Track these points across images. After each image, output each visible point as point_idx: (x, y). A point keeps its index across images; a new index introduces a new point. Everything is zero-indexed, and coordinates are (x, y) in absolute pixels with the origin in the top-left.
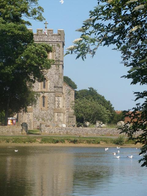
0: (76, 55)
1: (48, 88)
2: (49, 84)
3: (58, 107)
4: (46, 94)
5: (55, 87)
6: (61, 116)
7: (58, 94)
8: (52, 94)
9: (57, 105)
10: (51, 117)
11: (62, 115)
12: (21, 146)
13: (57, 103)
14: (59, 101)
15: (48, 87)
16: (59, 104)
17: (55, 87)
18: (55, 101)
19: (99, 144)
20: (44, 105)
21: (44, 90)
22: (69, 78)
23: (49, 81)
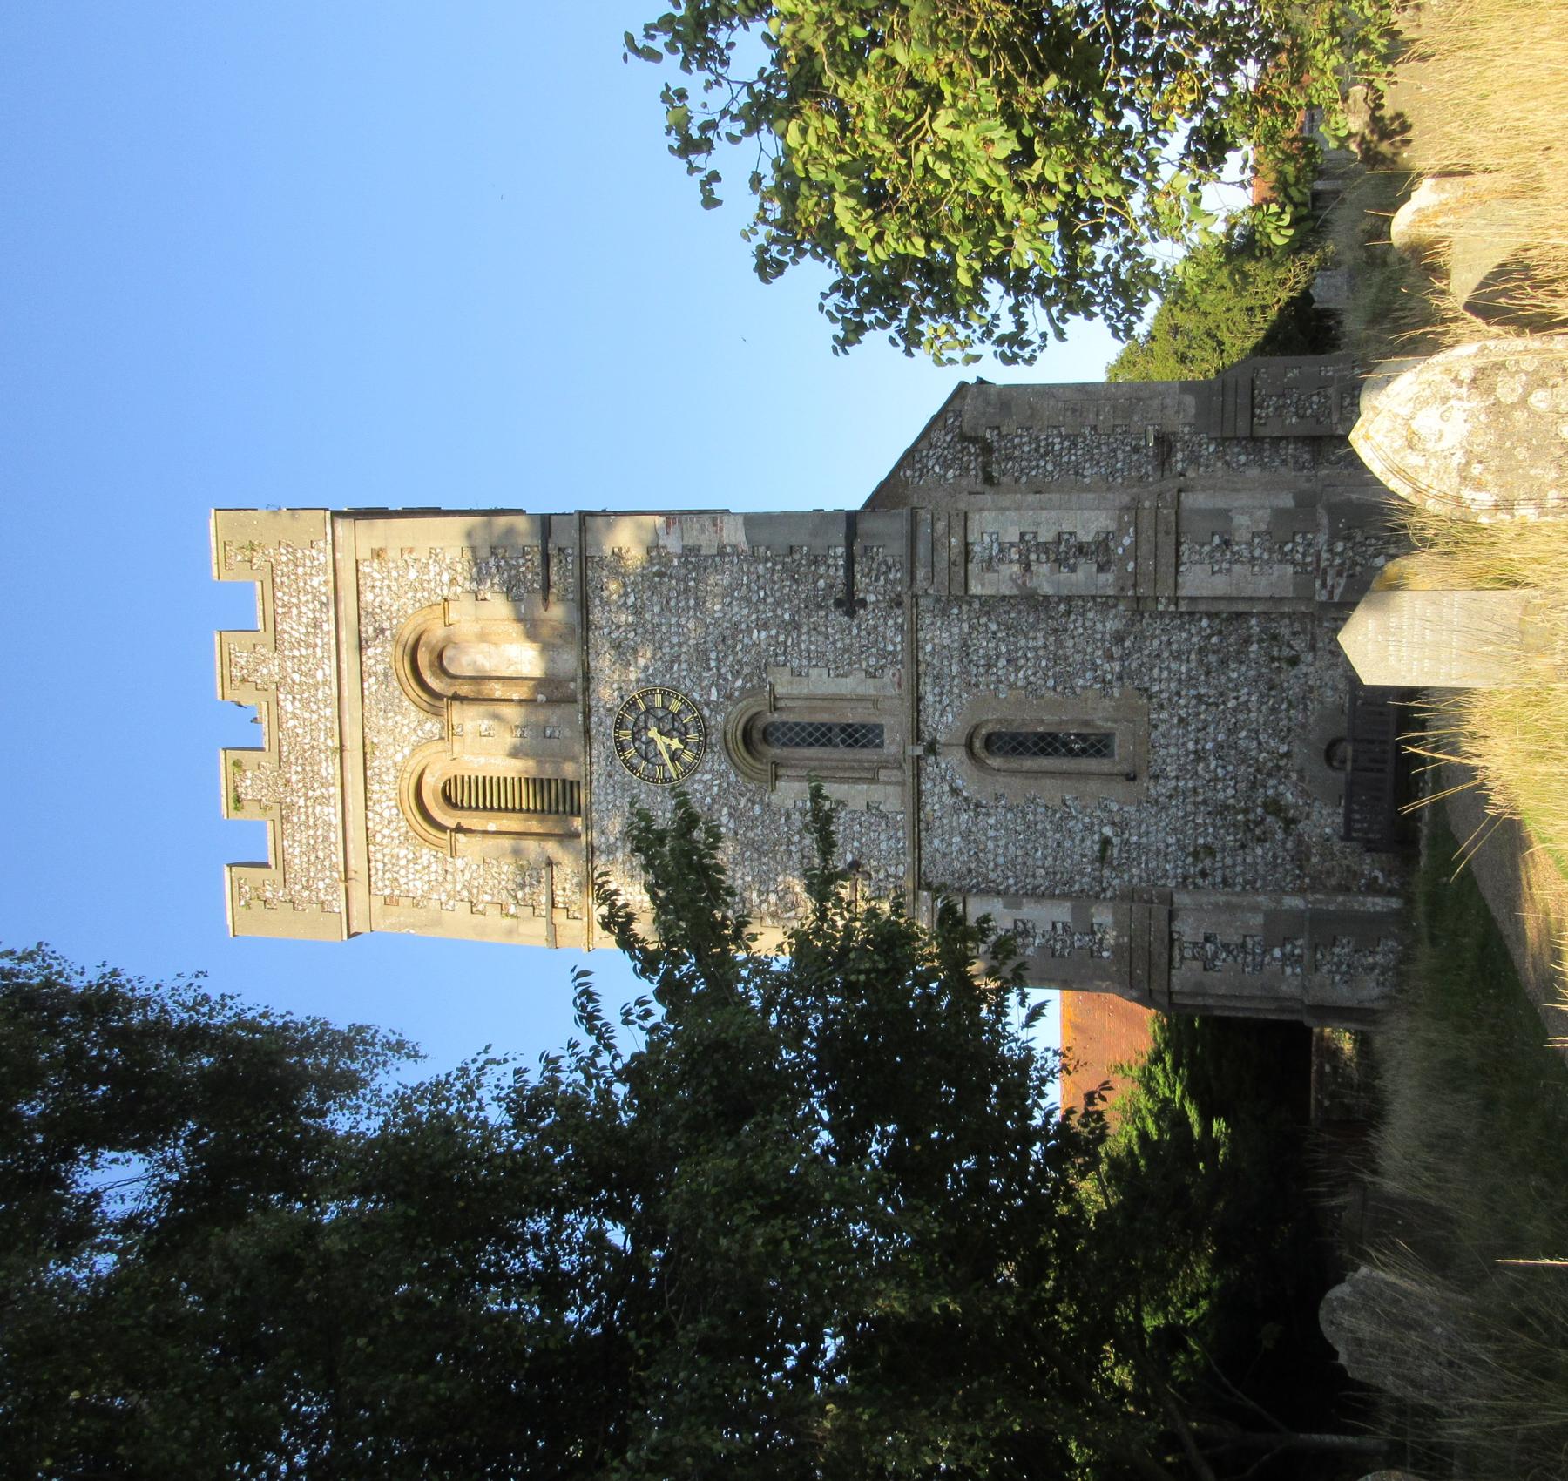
0: (237, 1000)
1: (869, 688)
2: (820, 682)
3: (1099, 551)
4: (944, 722)
5: (850, 603)
6: (1225, 514)
7: (942, 563)
8: (938, 636)
9: (1083, 577)
10: (1241, 656)
11: (1220, 502)
12: (1500, 925)
13: (1045, 579)
14: (1029, 549)
15: (851, 685)
16: (1065, 552)
17: (850, 603)
18: (1032, 601)
19: (232, 805)
20: (1098, 745)
21: (894, 742)
22: (83, 967)
23: (783, 684)
